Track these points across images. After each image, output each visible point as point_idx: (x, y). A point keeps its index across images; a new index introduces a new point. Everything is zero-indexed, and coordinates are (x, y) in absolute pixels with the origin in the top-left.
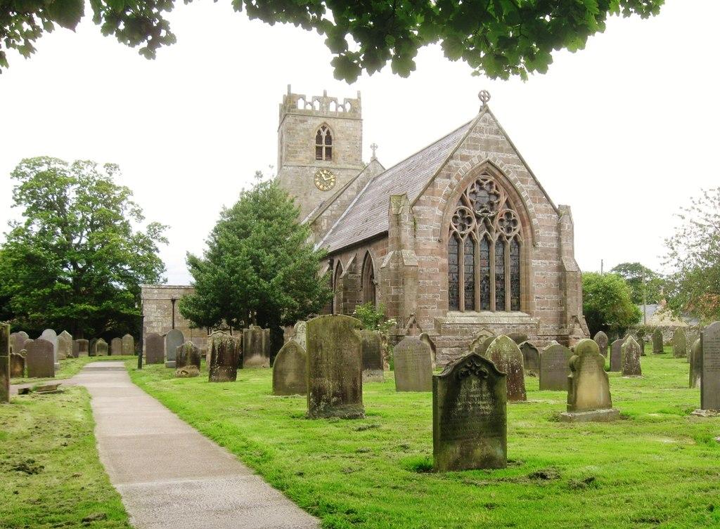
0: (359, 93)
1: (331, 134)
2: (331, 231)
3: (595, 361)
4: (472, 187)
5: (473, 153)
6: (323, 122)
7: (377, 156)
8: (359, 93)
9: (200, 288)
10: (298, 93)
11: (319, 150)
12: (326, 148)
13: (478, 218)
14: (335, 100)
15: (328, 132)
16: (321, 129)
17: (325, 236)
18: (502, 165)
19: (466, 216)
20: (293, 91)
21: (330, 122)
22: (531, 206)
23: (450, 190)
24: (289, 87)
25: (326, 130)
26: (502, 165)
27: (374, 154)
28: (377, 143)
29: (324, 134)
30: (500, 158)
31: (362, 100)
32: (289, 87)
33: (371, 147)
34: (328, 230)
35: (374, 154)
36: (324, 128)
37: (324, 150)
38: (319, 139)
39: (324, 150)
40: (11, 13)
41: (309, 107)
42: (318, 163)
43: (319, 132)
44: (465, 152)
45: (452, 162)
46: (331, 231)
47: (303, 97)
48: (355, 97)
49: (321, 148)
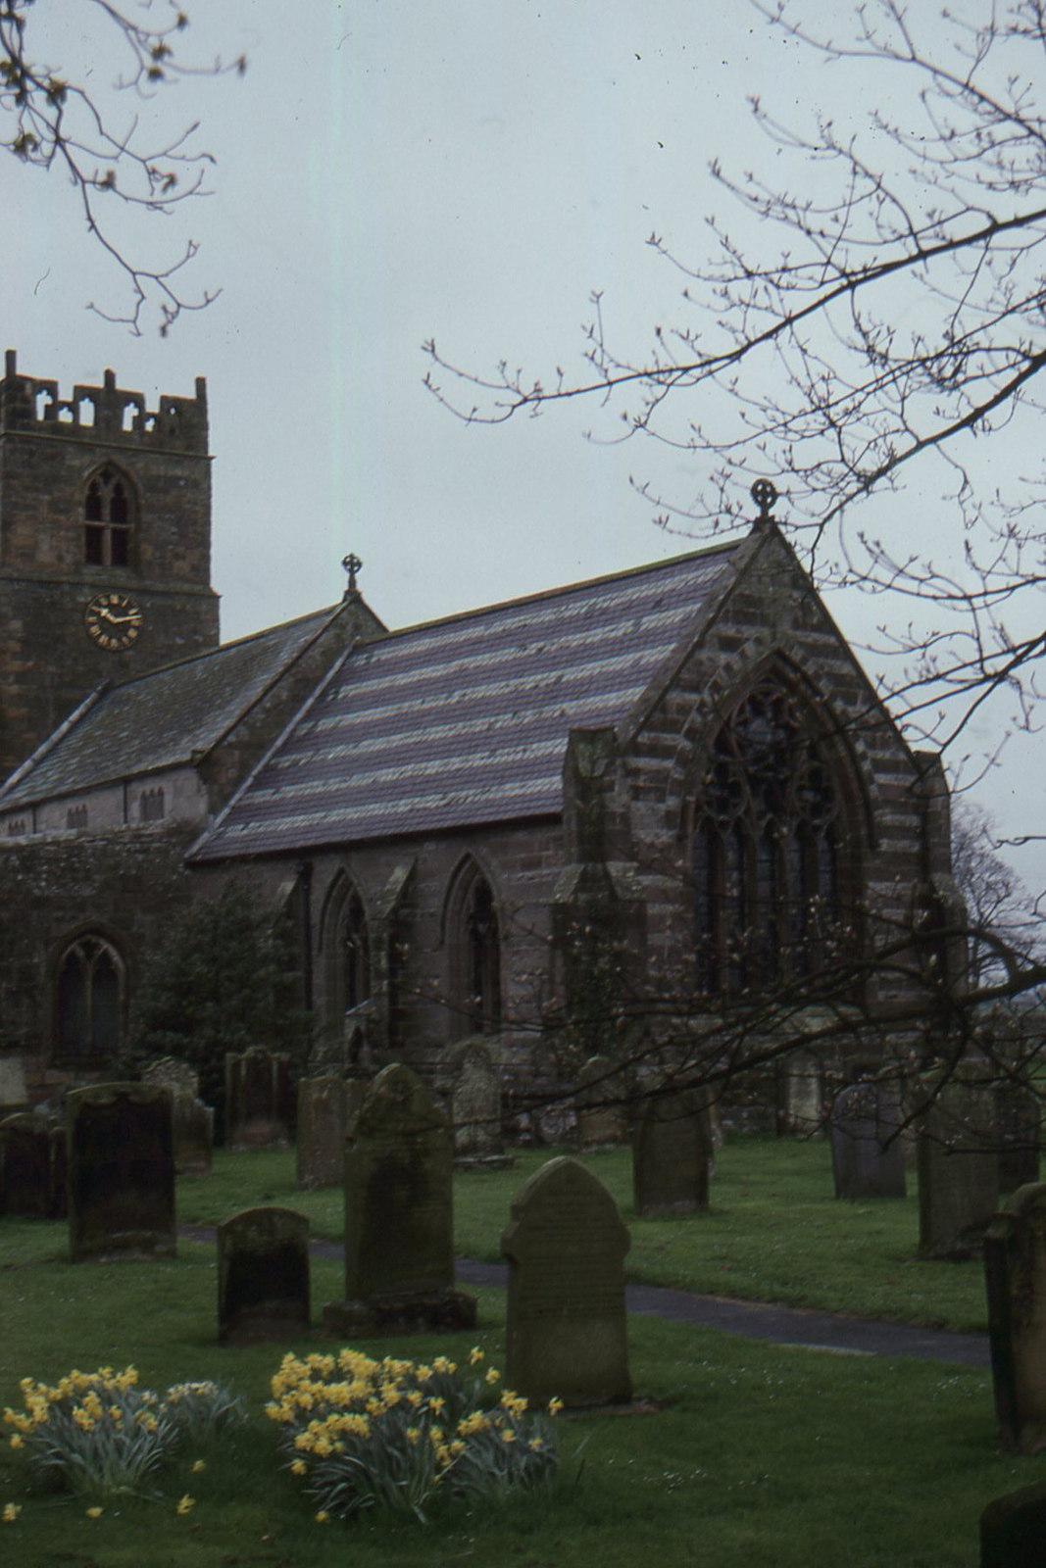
0: (201, 384)
1: (127, 494)
2: (249, 781)
3: (575, 869)
4: (742, 711)
5: (749, 631)
6: (104, 459)
7: (359, 587)
8: (201, 384)
9: (443, 1374)
10: (38, 374)
11: (93, 536)
12: (115, 532)
13: (754, 781)
14: (138, 400)
15: (118, 489)
16: (100, 480)
17: (232, 794)
18: (805, 660)
19: (731, 780)
20: (22, 369)
21: (121, 460)
22: (864, 756)
23: (699, 719)
24: (11, 356)
25: (114, 481)
26: (805, 660)
27: (352, 582)
28: (360, 555)
29: (107, 493)
30: (802, 644)
31: (210, 406)
32: (11, 356)
33: (345, 563)
34: (241, 779)
35: (352, 582)
36: (106, 476)
37: (108, 537)
38: (93, 507)
39: (108, 537)
40: (554, 1399)
41: (65, 416)
42: (90, 573)
43: (94, 487)
44: (729, 630)
45: (703, 655)
46: (249, 781)
47: (51, 387)
48: (190, 394)
49: (99, 531)
